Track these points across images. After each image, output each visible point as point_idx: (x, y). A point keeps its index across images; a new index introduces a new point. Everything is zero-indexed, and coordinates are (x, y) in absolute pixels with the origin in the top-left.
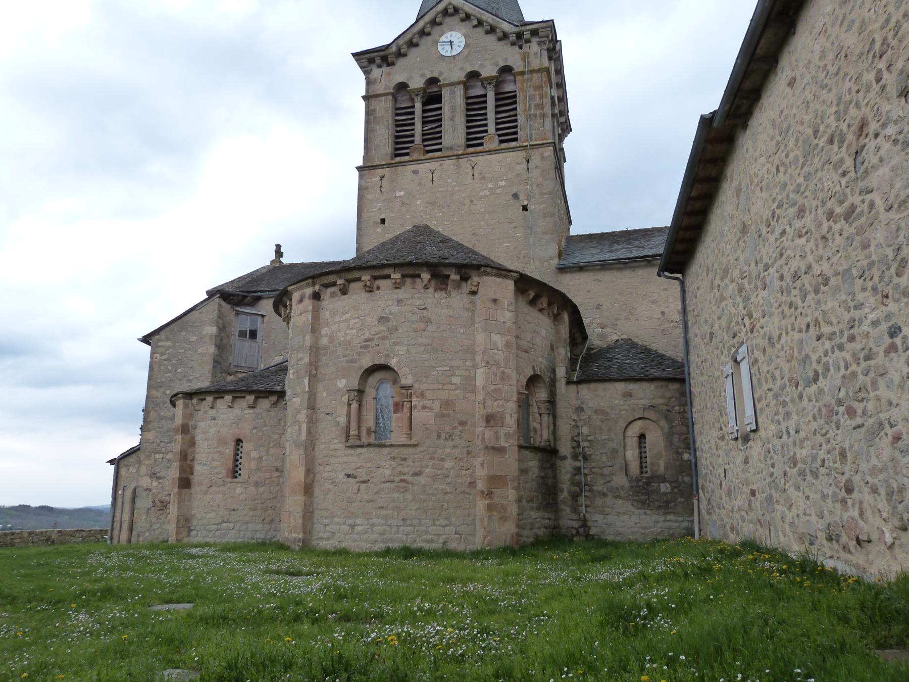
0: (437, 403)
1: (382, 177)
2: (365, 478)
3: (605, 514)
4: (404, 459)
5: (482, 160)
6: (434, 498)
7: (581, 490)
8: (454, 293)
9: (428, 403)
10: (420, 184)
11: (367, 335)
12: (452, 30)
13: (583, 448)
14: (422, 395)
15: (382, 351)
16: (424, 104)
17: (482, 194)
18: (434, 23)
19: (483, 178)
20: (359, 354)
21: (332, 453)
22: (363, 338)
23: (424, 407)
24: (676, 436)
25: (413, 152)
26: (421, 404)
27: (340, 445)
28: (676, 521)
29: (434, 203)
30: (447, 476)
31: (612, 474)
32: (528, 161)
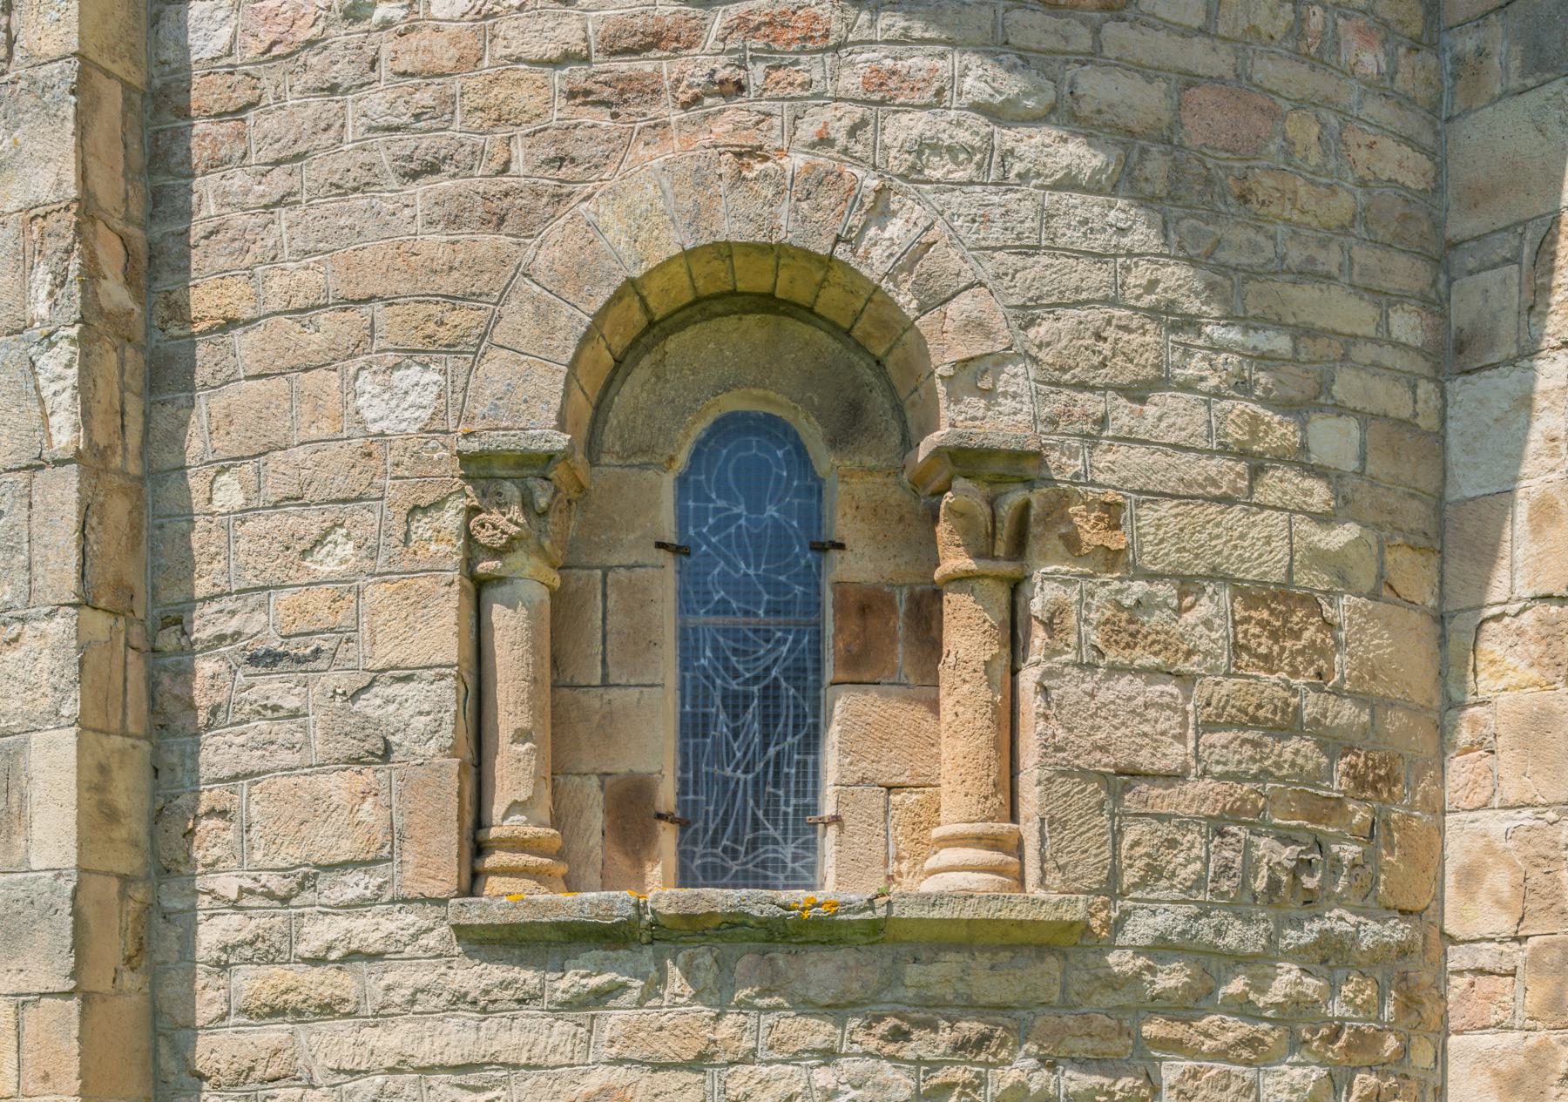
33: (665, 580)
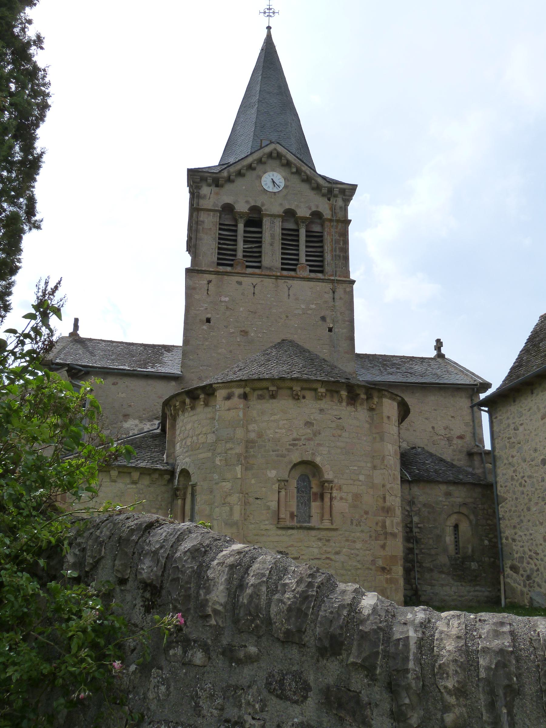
0: (350, 495)
1: (209, 282)
2: (296, 555)
3: (432, 585)
4: (328, 541)
5: (296, 284)
6: (349, 573)
7: (414, 566)
8: (359, 408)
9: (344, 495)
10: (243, 294)
11: (295, 436)
12: (273, 170)
13: (415, 533)
14: (340, 489)
15: (309, 450)
16: (245, 226)
17: (296, 312)
18: (260, 161)
19: (297, 299)
20: (289, 450)
21: (263, 532)
22: (291, 437)
23: (341, 498)
24: (480, 527)
25: (237, 265)
26: (339, 496)
27: (272, 526)
28: (481, 591)
29: (255, 313)
30: (357, 555)
31: (437, 554)
32: (334, 292)
33: (295, 490)
